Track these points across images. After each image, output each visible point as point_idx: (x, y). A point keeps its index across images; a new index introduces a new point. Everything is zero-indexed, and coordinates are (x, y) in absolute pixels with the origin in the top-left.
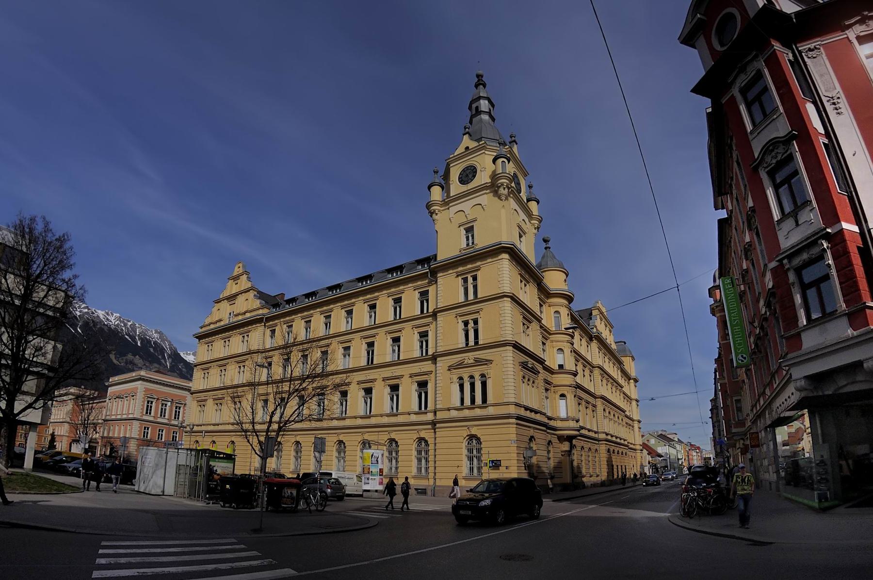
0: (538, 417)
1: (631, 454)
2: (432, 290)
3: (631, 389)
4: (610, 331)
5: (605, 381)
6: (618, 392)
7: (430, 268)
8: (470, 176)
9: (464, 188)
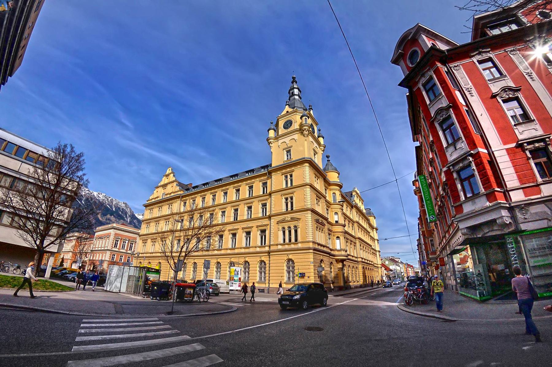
0: (325, 249)
2: (269, 182)
7: (268, 170)
9: (286, 131)
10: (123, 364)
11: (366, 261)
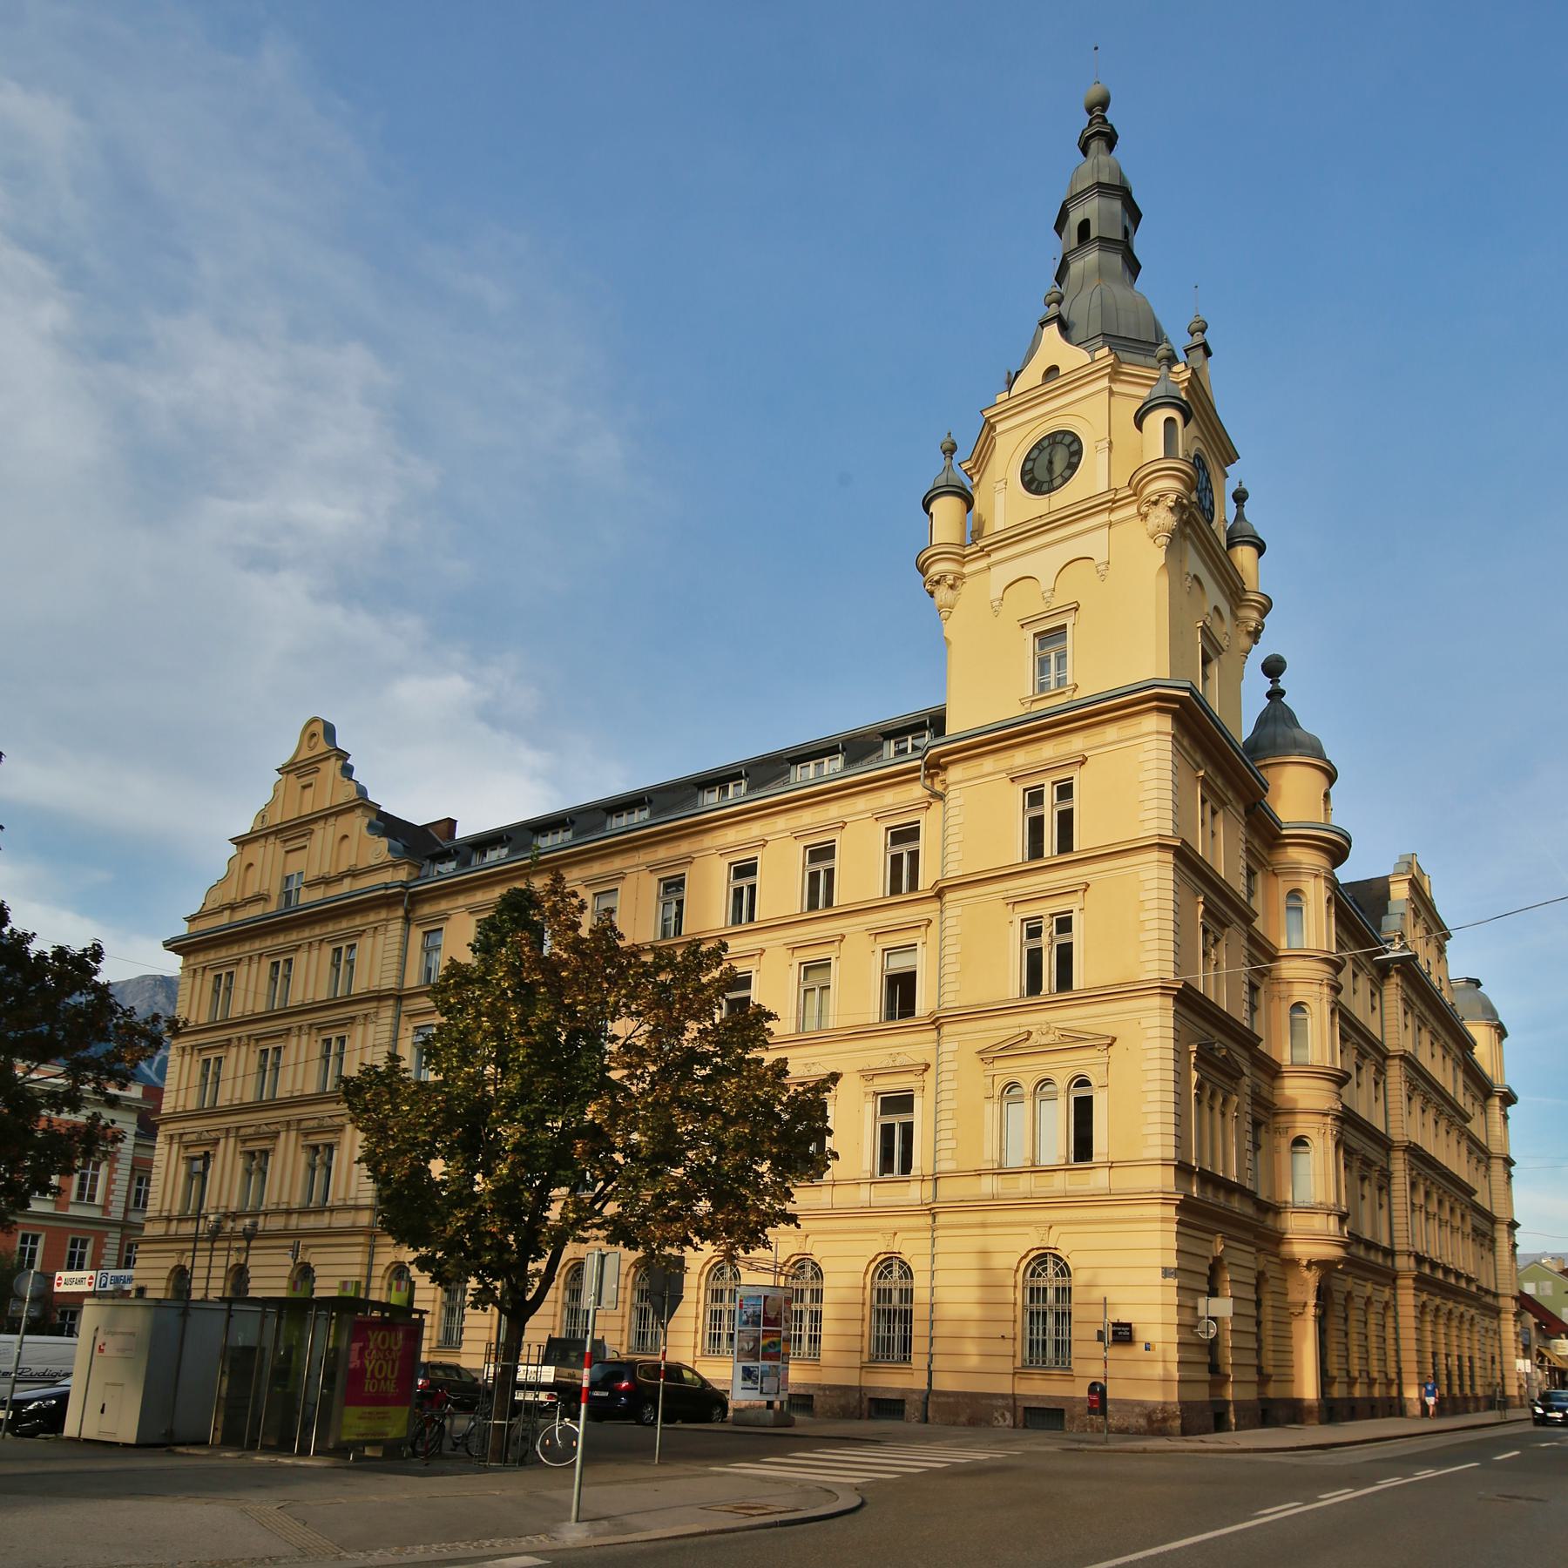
1: (1487, 1322)
2: (929, 824)
6: (1454, 1135)
7: (919, 741)
8: (1059, 467)
9: (1038, 506)
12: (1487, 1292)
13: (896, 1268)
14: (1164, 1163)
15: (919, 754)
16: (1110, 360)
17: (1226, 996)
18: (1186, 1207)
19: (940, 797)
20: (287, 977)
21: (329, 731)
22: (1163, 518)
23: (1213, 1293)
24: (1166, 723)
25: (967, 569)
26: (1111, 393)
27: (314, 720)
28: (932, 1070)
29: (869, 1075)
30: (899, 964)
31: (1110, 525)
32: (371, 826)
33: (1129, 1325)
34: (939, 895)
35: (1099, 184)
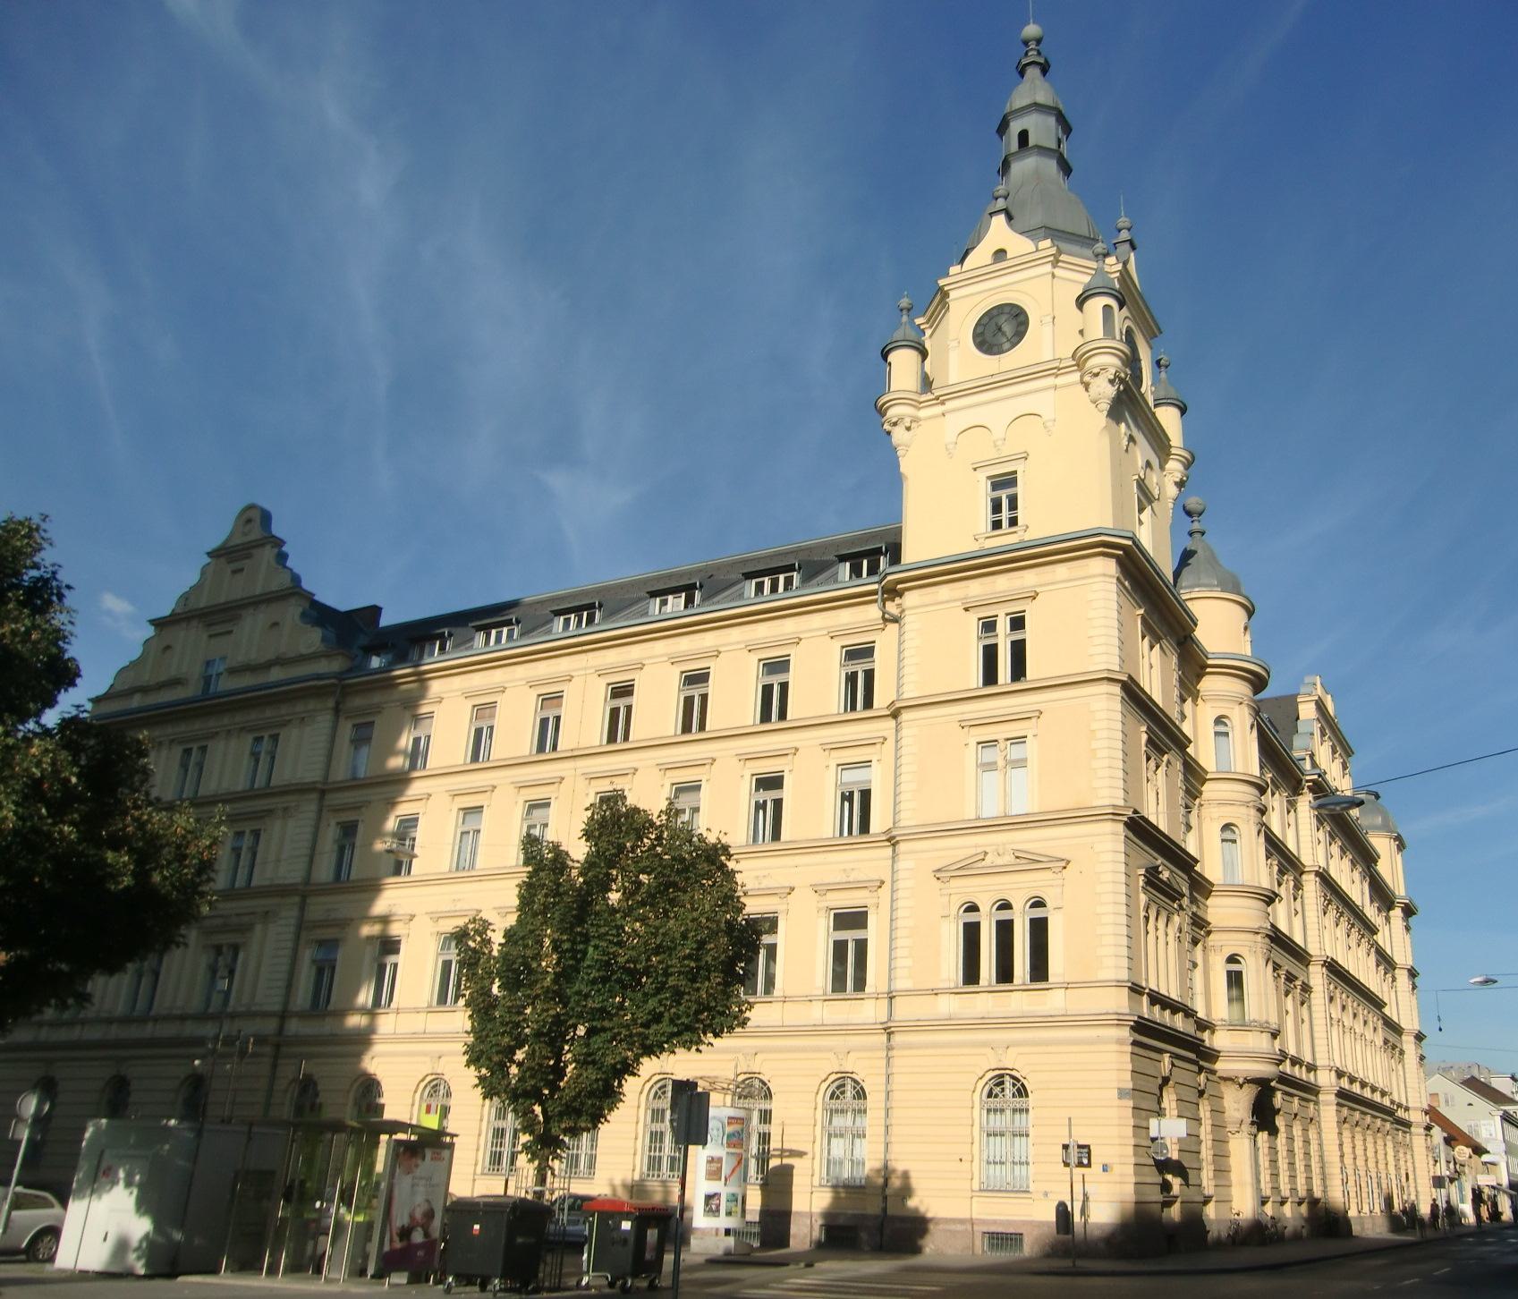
0: (1179, 1022)
2: (885, 643)
3: (1394, 935)
4: (1345, 767)
5: (1332, 913)
6: (1364, 945)
9: (989, 365)
10: (326, 999)
11: (1367, 1093)
12: (1400, 1106)
13: (849, 1088)
14: (1118, 984)
15: (876, 578)
16: (1053, 250)
17: (1159, 816)
18: (1142, 1027)
19: (896, 620)
20: (200, 766)
21: (266, 517)
22: (1105, 390)
23: (1160, 1113)
24: (1111, 566)
25: (923, 413)
26: (1054, 276)
27: (252, 507)
28: (887, 887)
29: (820, 890)
30: (854, 778)
31: (1056, 388)
32: (304, 615)
33: (1088, 1147)
34: (895, 715)
35: (1036, 104)
